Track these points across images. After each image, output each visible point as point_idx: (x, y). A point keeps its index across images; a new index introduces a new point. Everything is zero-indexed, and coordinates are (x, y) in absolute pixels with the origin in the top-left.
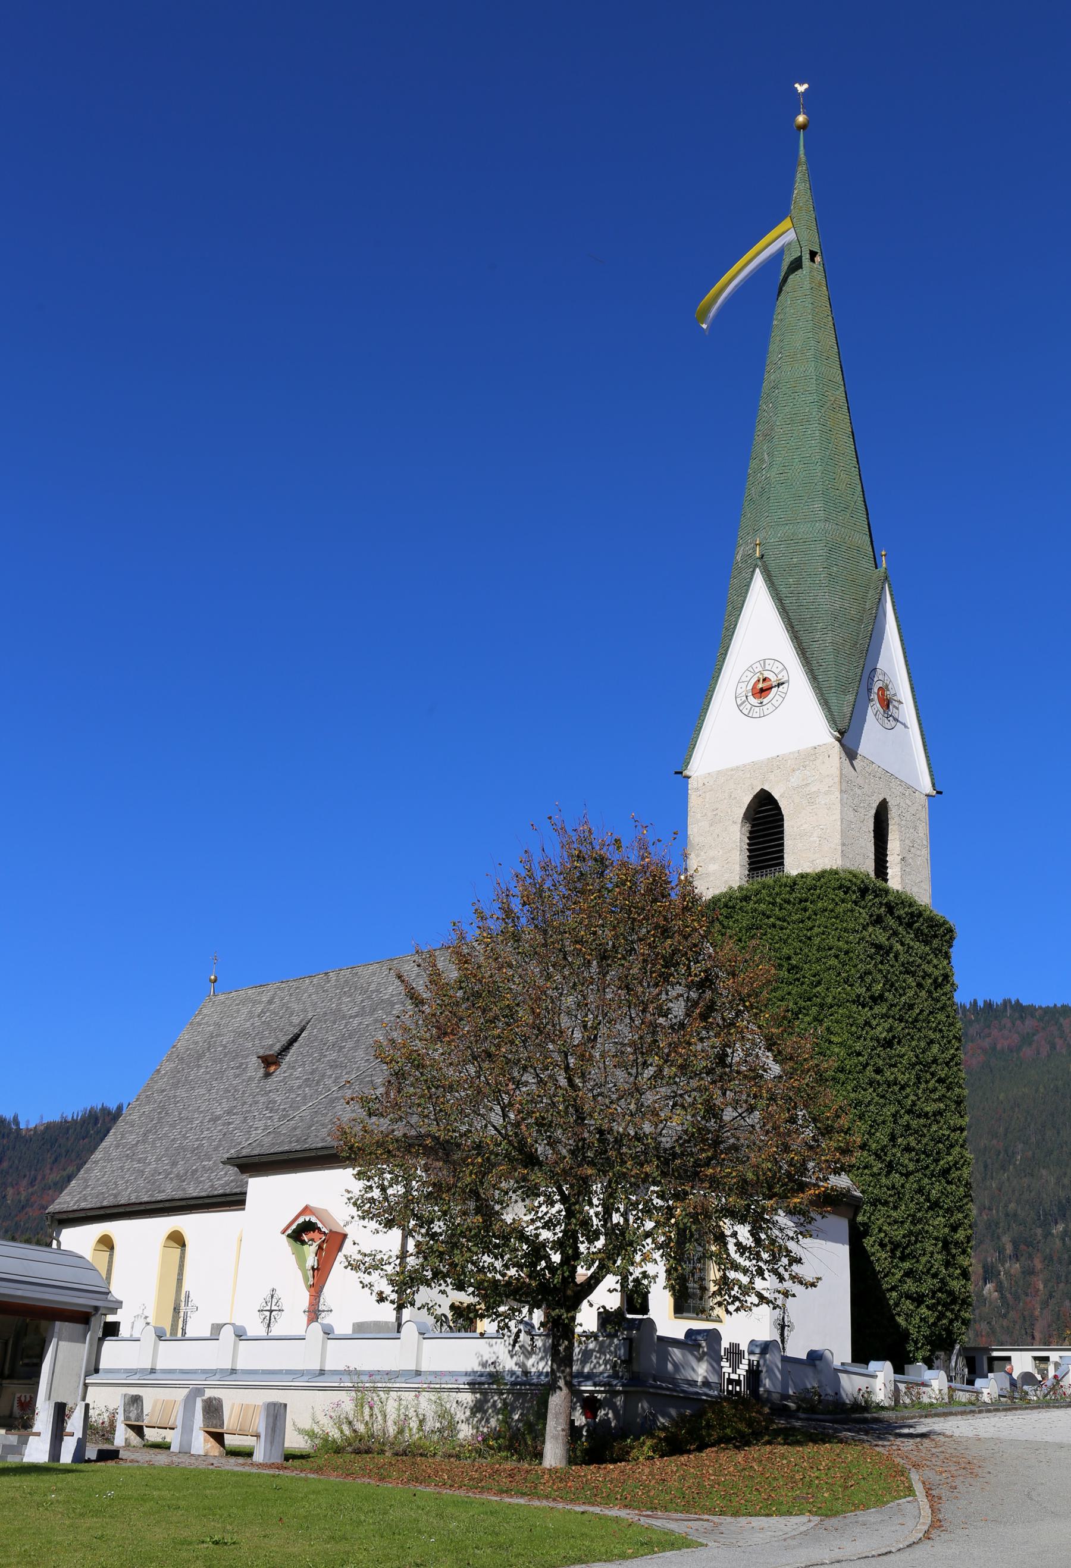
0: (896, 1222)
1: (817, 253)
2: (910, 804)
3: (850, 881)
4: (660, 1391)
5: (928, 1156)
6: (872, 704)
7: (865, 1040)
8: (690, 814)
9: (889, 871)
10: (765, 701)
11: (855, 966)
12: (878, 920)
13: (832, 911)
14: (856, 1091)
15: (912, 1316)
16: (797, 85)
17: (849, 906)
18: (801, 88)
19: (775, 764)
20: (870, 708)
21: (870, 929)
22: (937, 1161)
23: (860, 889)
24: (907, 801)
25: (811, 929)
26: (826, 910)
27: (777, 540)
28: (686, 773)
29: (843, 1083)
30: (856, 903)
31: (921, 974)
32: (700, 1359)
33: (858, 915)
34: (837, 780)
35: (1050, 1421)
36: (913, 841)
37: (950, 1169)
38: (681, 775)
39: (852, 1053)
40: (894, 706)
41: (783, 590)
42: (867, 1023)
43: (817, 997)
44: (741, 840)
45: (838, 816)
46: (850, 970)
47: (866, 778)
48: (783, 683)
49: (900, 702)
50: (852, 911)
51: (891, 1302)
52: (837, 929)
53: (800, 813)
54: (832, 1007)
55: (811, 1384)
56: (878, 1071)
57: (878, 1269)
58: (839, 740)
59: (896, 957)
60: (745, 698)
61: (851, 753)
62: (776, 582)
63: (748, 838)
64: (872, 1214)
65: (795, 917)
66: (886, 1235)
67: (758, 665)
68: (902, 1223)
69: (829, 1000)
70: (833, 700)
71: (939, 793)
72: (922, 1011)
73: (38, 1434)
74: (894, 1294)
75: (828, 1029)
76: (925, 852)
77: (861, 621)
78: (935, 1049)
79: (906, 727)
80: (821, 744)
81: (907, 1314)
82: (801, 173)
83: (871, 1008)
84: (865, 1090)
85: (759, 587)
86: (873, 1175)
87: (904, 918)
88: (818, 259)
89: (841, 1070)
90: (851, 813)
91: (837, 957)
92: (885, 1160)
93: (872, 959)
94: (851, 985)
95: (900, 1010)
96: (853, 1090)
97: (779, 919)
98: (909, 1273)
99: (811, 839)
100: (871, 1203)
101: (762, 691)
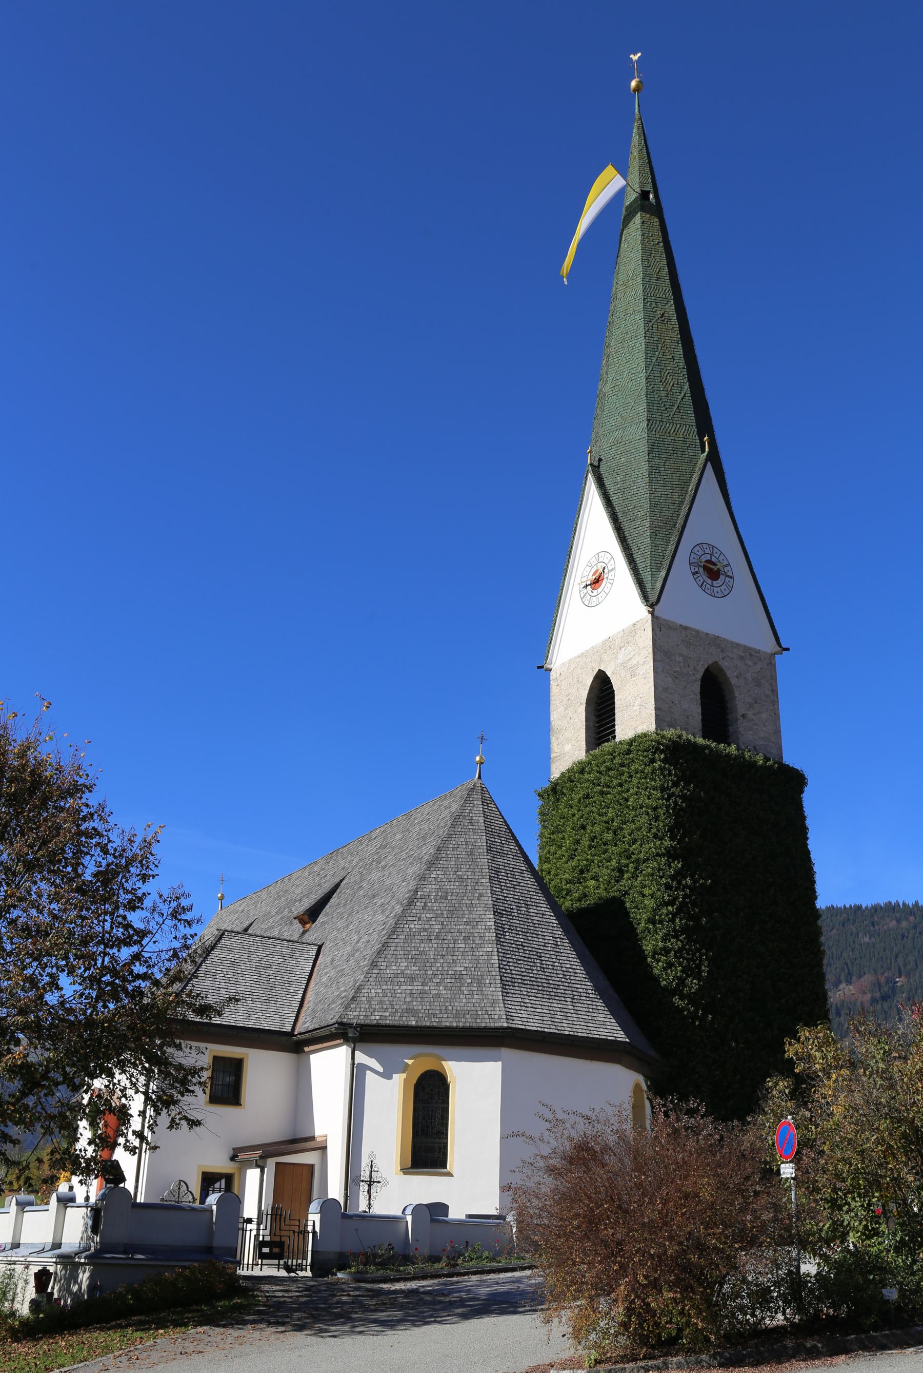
16: (632, 56)
18: (635, 58)
19: (608, 645)
25: (628, 790)
27: (609, 445)
34: (651, 650)
35: (210, 1344)
38: (543, 670)
55: (53, 1288)
65: (615, 782)
67: (697, 580)
80: (638, 620)
91: (648, 814)
101: (597, 582)
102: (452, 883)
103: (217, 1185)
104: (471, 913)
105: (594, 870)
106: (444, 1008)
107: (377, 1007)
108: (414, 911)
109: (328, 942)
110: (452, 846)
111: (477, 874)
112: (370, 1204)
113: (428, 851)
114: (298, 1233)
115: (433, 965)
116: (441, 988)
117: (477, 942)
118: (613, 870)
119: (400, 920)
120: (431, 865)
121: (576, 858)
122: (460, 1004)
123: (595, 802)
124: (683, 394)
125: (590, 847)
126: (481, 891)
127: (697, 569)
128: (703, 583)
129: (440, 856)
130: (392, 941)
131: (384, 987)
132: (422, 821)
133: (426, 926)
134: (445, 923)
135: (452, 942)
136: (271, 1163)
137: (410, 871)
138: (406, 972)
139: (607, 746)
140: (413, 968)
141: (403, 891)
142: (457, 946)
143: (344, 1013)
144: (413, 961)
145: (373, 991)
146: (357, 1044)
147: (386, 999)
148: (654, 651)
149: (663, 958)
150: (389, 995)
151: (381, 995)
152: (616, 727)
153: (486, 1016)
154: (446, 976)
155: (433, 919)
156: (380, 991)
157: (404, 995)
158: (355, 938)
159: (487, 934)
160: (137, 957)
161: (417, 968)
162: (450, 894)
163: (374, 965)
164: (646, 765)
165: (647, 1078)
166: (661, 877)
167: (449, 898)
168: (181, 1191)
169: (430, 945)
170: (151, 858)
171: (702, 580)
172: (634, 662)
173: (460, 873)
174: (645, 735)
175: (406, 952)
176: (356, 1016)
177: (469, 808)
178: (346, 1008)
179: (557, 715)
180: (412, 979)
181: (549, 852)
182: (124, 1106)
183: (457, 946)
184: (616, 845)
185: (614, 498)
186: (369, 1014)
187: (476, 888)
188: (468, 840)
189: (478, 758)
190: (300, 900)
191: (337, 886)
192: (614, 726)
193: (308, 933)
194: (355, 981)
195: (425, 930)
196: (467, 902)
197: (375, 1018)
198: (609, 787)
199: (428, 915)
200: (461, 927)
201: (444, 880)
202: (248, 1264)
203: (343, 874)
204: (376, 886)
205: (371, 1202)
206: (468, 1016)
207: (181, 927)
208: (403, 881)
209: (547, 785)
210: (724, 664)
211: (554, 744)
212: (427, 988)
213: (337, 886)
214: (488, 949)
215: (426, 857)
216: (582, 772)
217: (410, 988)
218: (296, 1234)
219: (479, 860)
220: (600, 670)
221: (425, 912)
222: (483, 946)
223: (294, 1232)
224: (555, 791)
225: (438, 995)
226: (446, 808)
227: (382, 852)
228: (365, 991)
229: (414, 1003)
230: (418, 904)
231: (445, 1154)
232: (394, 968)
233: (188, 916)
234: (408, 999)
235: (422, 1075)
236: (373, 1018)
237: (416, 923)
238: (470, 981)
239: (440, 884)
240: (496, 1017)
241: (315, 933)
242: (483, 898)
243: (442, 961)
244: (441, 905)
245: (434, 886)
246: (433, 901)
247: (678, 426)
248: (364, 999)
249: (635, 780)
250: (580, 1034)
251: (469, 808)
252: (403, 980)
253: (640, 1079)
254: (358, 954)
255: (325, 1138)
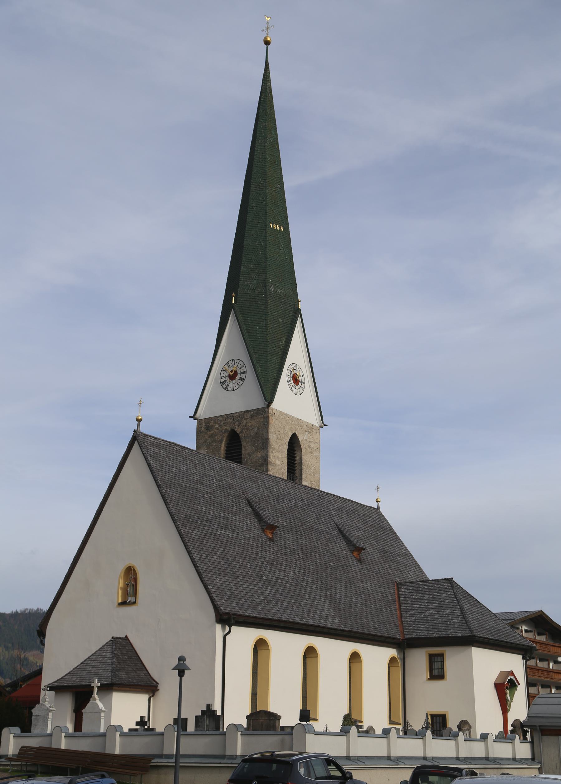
19: (299, 422)
127: (290, 380)
172: (312, 446)
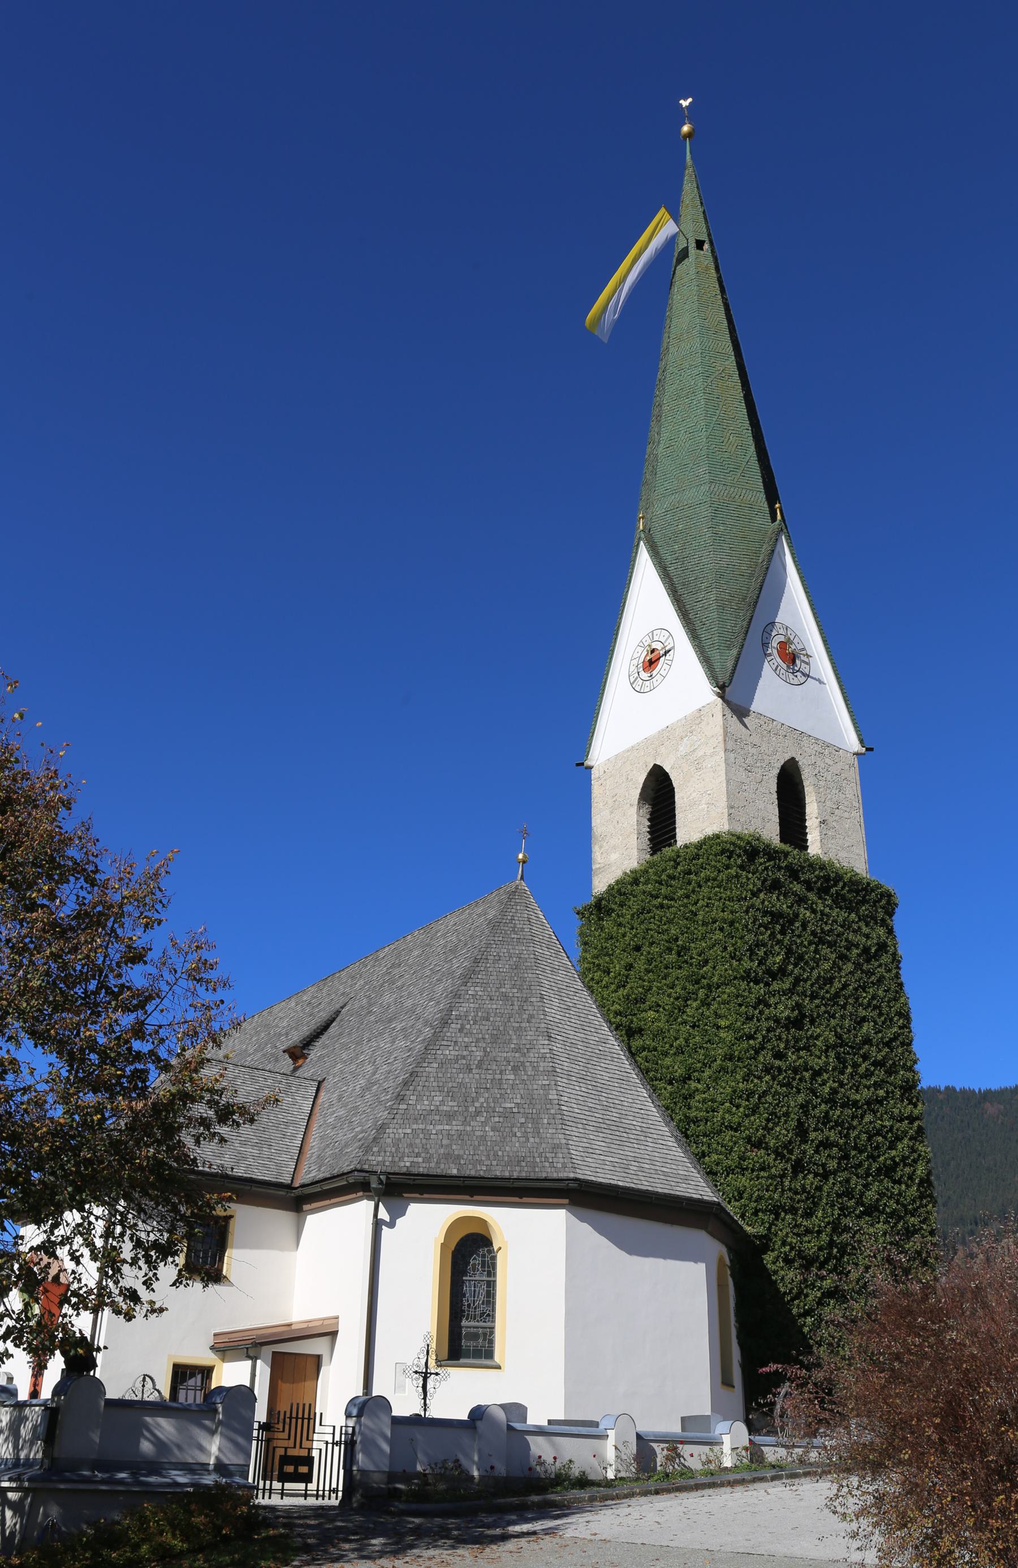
0: (808, 1231)
1: (704, 241)
2: (831, 763)
3: (733, 844)
4: (92, 1487)
5: (861, 1152)
6: (769, 658)
7: (758, 1021)
8: (594, 805)
9: (809, 837)
10: (655, 673)
11: (742, 938)
12: (775, 886)
13: (715, 879)
14: (747, 1081)
15: (839, 1346)
16: (682, 102)
17: (733, 871)
18: (685, 103)
19: (666, 736)
20: (766, 663)
21: (762, 895)
22: (874, 1158)
23: (745, 851)
24: (827, 760)
25: (696, 903)
26: (709, 880)
27: (664, 511)
28: (588, 763)
29: (732, 1072)
30: (742, 867)
31: (843, 943)
32: (212, 1433)
33: (744, 881)
34: (721, 738)
36: (838, 803)
37: (896, 1164)
39: (741, 1037)
40: (804, 661)
41: (668, 558)
42: (760, 1001)
43: (705, 978)
44: (639, 823)
45: (723, 778)
46: (736, 943)
47: (763, 736)
48: (669, 651)
49: (808, 656)
50: (737, 876)
51: (806, 1330)
52: (721, 898)
53: (689, 782)
54: (719, 987)
56: (779, 1055)
57: (782, 1290)
58: (722, 696)
59: (804, 926)
60: (637, 675)
61: (739, 710)
62: (661, 551)
63: (649, 820)
64: (771, 1225)
65: (680, 893)
66: (792, 1248)
68: (819, 1232)
69: (715, 979)
70: (715, 656)
71: (868, 749)
72: (845, 986)
73: (282, 1498)
74: (809, 1320)
75: (716, 1013)
76: (857, 816)
77: (752, 575)
78: (866, 1028)
79: (820, 682)
81: (830, 1344)
82: (689, 171)
83: (767, 984)
84: (760, 1078)
85: (644, 559)
86: (772, 1177)
87: (815, 883)
88: (706, 246)
89: (730, 1058)
90: (742, 775)
91: (721, 929)
92: (789, 1159)
93: (767, 929)
94: (739, 960)
95: (812, 985)
96: (744, 1080)
97: (666, 897)
98: (833, 1293)
99: (700, 807)
100: (770, 1211)
101: (651, 664)
102: (494, 1002)
103: (191, 1382)
104: (519, 1037)
105: (652, 999)
106: (492, 1153)
107: (407, 1151)
108: (449, 1034)
109: (331, 1078)
110: (492, 957)
111: (524, 991)
112: (425, 1404)
113: (460, 964)
114: (333, 1444)
115: (475, 1099)
116: (487, 1129)
117: (529, 1073)
118: (677, 999)
119: (430, 1045)
120: (467, 978)
121: (629, 986)
122: (514, 1146)
123: (654, 918)
124: (748, 458)
125: (648, 971)
126: (531, 1012)
128: (777, 666)
129: (477, 969)
130: (422, 1069)
131: (415, 1126)
132: (447, 933)
133: (465, 1053)
134: (488, 1050)
135: (498, 1072)
136: (267, 1351)
137: (439, 989)
138: (441, 1108)
139: (667, 851)
140: (450, 1104)
141: (432, 1011)
142: (505, 1077)
143: (365, 1158)
144: (451, 1094)
145: (400, 1131)
146: (382, 1198)
147: (418, 1141)
148: (725, 740)
149: (744, 1103)
150: (421, 1136)
151: (411, 1136)
152: (677, 830)
153: (547, 1164)
154: (492, 1114)
155: (474, 1044)
156: (409, 1131)
157: (440, 1137)
158: (370, 1068)
159: (542, 1064)
160: (138, 1031)
161: (455, 1104)
162: (492, 1015)
163: (400, 1098)
164: (719, 871)
165: (730, 1249)
166: (740, 1005)
167: (491, 1019)
168: (145, 1389)
169: (471, 1075)
170: (159, 895)
171: (776, 664)
172: (700, 753)
173: (504, 990)
174: (717, 836)
175: (441, 1084)
176: (380, 1161)
177: (511, 914)
178: (367, 1152)
179: (600, 819)
180: (450, 1116)
181: (592, 979)
182: (114, 1248)
183: (505, 1077)
184: (680, 968)
185: (671, 569)
186: (397, 1159)
187: (525, 1008)
188: (511, 951)
189: (521, 856)
190: (287, 1034)
191: (338, 1013)
192: (675, 828)
193: (301, 1070)
194: (376, 1120)
195: (464, 1057)
196: (514, 1024)
197: (405, 1164)
198: (672, 899)
199: (466, 1039)
200: (509, 1054)
201: (485, 997)
202: (324, 1490)
203: (342, 1000)
204: (393, 1008)
205: (428, 1402)
206: (523, 1164)
207: (201, 990)
208: (431, 1000)
209: (593, 900)
210: (803, 762)
211: (597, 853)
212: (468, 1128)
213: (338, 1013)
214: (544, 1082)
215: (460, 971)
216: (636, 882)
217: (447, 1127)
218: (330, 1446)
219: (526, 975)
220: (655, 765)
221: (463, 1035)
222: (536, 1077)
223: (327, 1443)
224: (600, 908)
225: (483, 1138)
226: (479, 915)
227: (396, 971)
228: (391, 1131)
229: (454, 1147)
230: (453, 1026)
231: (491, 1342)
232: (426, 1103)
233: (212, 975)
234: (445, 1142)
235: (462, 1239)
236: (402, 1164)
237: (451, 1048)
238: (523, 1120)
239: (480, 1002)
240: (559, 1165)
241: (309, 1068)
242: (533, 1021)
243: (487, 1095)
244: (482, 1027)
245: (472, 1005)
246: (472, 1022)
247: (744, 491)
248: (389, 1141)
249: (705, 890)
250: (660, 1190)
251: (511, 914)
252: (437, 1118)
253: (724, 1250)
254: (375, 1087)
255: (335, 1321)
